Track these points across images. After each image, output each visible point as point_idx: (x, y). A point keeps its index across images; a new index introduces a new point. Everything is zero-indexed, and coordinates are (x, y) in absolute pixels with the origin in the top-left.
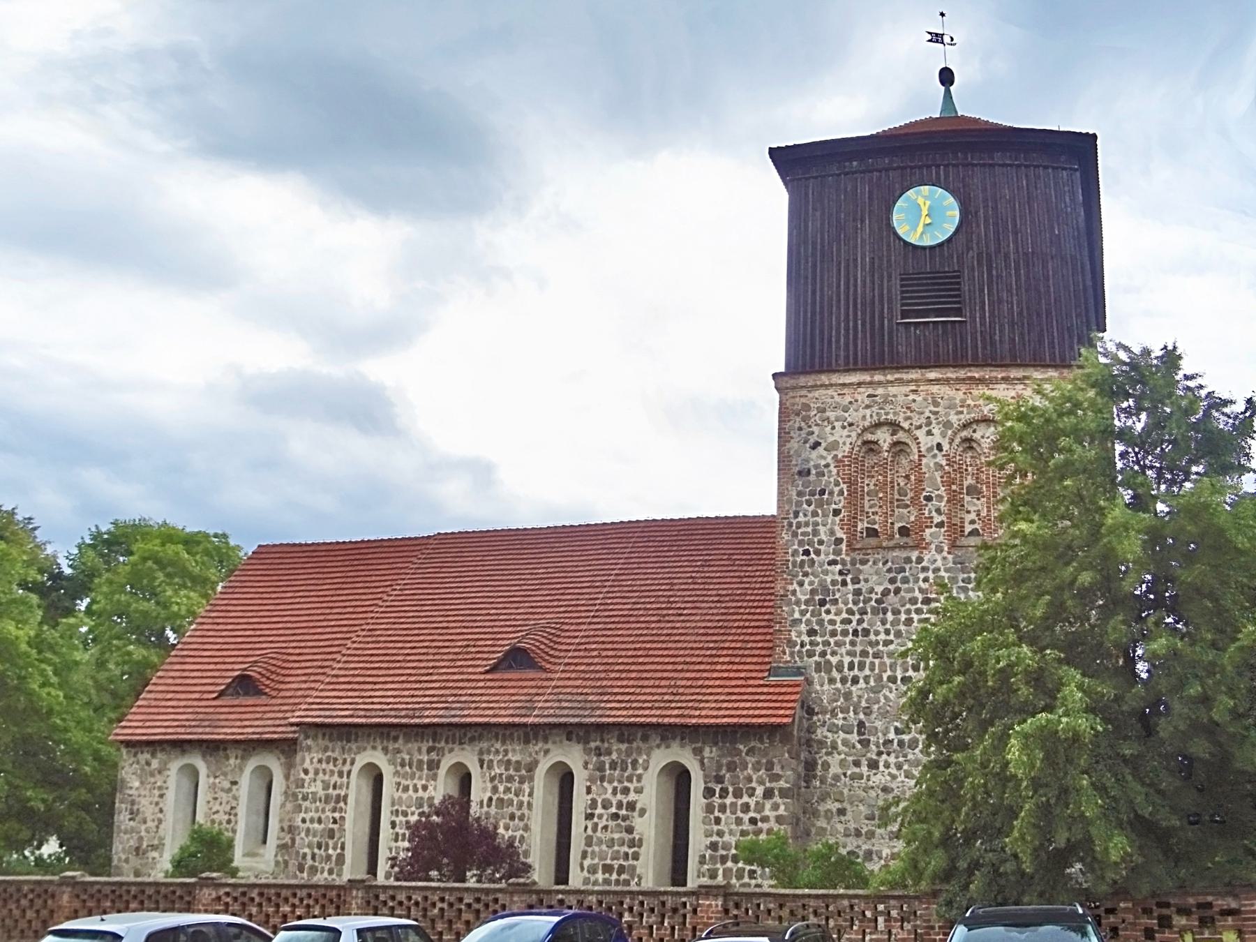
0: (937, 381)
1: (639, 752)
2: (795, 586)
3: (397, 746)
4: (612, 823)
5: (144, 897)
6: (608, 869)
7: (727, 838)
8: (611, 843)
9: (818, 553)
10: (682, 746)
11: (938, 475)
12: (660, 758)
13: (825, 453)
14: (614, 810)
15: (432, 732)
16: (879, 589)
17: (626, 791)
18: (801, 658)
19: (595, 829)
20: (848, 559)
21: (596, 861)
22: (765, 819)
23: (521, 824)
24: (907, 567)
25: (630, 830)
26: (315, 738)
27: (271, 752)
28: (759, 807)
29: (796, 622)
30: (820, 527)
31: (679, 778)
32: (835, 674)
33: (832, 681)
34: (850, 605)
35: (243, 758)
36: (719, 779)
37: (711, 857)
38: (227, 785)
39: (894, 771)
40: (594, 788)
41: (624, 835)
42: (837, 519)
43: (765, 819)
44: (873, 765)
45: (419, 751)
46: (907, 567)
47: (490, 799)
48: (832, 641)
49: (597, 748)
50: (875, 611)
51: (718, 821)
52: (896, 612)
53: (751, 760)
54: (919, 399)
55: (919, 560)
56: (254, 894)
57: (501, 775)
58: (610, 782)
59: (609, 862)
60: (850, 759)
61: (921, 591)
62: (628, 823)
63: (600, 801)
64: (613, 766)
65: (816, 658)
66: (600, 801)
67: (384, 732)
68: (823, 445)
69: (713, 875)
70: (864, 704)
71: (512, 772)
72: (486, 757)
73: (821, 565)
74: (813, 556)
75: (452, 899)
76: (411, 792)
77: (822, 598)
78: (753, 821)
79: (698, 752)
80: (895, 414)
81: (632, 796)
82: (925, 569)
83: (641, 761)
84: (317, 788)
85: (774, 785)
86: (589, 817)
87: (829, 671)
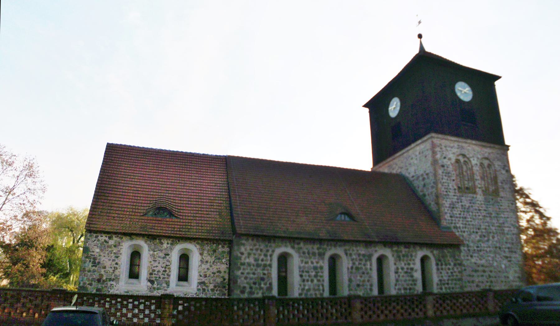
0: (475, 144)
1: (412, 251)
6: (405, 289)
8: (405, 281)
12: (420, 253)
15: (368, 243)
16: (467, 205)
19: (399, 276)
22: (455, 272)
25: (412, 276)
26: (247, 240)
27: (191, 243)
28: (453, 269)
31: (424, 260)
36: (440, 260)
38: (162, 255)
41: (410, 278)
44: (472, 256)
47: (352, 268)
50: (468, 212)
51: (441, 273)
52: (472, 213)
58: (403, 261)
64: (404, 256)
71: (361, 257)
77: (453, 207)
79: (432, 252)
81: (412, 266)
84: (251, 260)
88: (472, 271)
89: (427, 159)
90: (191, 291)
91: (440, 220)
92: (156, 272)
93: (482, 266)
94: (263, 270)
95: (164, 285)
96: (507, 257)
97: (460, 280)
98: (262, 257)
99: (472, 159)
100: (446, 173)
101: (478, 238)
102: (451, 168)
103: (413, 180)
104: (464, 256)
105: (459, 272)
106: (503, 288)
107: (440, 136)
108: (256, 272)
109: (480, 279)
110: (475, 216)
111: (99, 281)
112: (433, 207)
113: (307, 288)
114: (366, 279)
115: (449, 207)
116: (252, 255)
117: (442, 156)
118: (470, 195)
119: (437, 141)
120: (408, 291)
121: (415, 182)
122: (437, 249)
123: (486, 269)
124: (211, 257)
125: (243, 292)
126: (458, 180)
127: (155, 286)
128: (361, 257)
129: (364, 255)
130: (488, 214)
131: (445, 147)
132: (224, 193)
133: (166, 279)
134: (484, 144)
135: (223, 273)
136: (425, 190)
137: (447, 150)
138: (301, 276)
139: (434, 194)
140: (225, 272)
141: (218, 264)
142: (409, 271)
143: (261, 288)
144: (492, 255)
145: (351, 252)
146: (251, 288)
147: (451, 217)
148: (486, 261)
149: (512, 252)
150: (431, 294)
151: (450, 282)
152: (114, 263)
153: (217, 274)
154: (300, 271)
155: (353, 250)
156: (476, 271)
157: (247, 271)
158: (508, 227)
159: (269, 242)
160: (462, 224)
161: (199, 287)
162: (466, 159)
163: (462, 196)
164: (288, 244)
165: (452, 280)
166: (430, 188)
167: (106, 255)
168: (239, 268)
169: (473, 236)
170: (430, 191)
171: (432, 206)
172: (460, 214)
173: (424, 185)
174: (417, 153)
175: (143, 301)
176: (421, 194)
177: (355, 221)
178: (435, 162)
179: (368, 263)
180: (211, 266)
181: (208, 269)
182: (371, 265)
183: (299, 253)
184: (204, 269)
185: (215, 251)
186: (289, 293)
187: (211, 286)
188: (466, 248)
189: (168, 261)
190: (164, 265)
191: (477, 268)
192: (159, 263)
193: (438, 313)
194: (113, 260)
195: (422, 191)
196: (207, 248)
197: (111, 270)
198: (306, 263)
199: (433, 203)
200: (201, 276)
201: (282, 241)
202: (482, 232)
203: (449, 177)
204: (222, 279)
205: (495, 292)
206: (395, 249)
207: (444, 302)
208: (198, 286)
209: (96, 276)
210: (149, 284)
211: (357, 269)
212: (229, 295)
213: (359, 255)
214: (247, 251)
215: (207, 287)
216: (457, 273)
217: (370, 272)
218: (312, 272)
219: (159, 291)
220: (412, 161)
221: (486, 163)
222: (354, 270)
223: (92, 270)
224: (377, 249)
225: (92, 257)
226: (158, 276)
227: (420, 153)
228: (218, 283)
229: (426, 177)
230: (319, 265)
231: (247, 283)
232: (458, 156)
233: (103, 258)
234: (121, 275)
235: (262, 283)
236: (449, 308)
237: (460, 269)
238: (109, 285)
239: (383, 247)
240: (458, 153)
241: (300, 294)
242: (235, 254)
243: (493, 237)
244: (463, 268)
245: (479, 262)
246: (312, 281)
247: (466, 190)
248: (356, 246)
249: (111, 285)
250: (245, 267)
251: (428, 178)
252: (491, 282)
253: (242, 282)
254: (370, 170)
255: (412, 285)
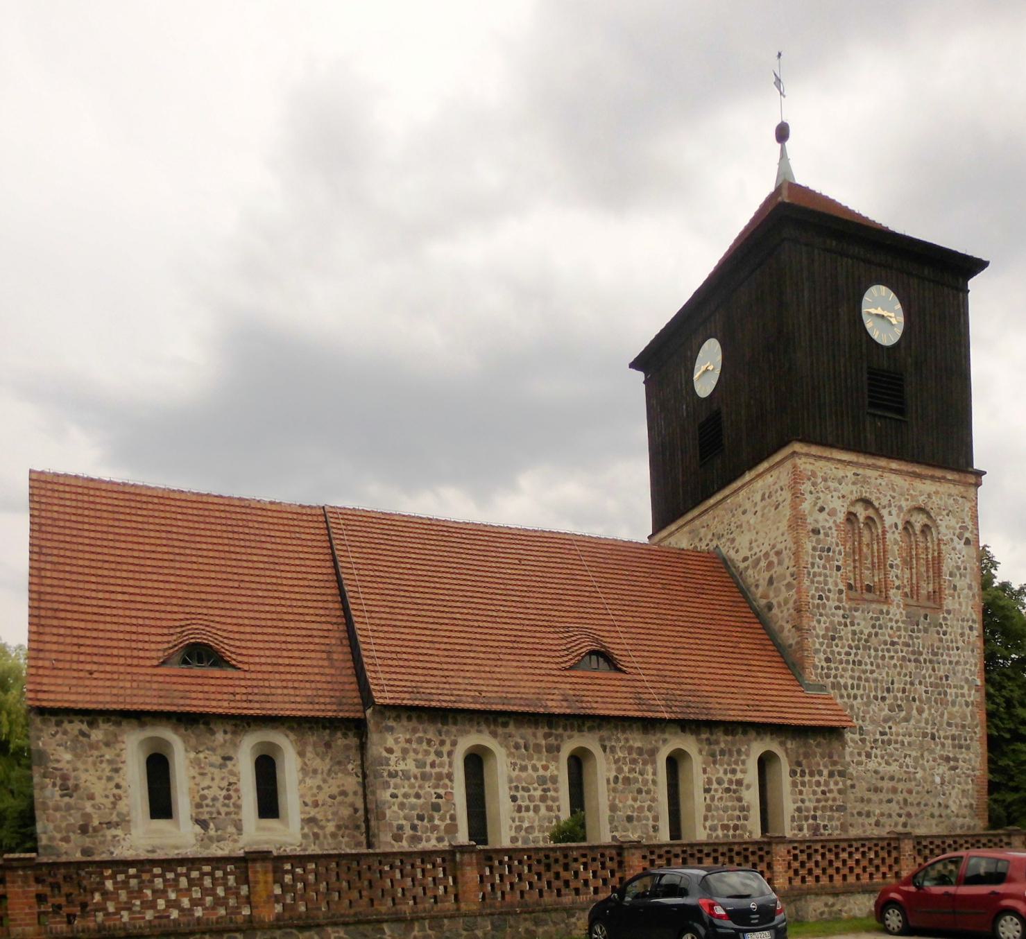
2: (815, 623)
3: (507, 730)
4: (725, 795)
5: (718, 854)
6: (725, 827)
7: (807, 804)
8: (725, 809)
9: (828, 599)
10: (772, 739)
11: (896, 548)
12: (758, 747)
13: (828, 517)
14: (726, 785)
15: (649, 725)
16: (866, 632)
17: (734, 772)
18: (822, 678)
19: (712, 799)
20: (847, 606)
21: (716, 822)
22: (831, 791)
23: (649, 797)
24: (881, 617)
25: (740, 799)
27: (277, 728)
28: (827, 783)
29: (817, 651)
30: (828, 579)
31: (765, 762)
32: (843, 691)
33: (842, 697)
34: (850, 642)
35: (234, 733)
36: (799, 764)
37: (799, 817)
38: (216, 759)
39: (879, 760)
40: (708, 769)
41: (737, 804)
42: (839, 573)
43: (831, 791)
44: (868, 756)
45: (538, 736)
46: (881, 617)
47: (616, 778)
48: (840, 667)
49: (708, 739)
50: (865, 648)
51: (801, 793)
52: (876, 650)
53: (818, 750)
54: (884, 483)
55: (888, 613)
56: (818, 846)
57: (624, 758)
58: (721, 765)
59: (726, 822)
60: (856, 751)
61: (890, 636)
62: (737, 794)
63: (714, 779)
64: (722, 753)
65: (832, 679)
66: (714, 779)
67: (687, 725)
68: (827, 510)
69: (801, 829)
70: (861, 714)
71: (634, 756)
72: (607, 743)
73: (831, 609)
74: (825, 600)
75: (973, 841)
76: (530, 771)
78: (824, 793)
79: (782, 744)
80: (870, 493)
81: (739, 776)
82: (891, 620)
83: (743, 750)
84: (410, 765)
85: (834, 768)
86: (707, 791)
87: (840, 689)
88: (869, 790)
89: (799, 508)
90: (289, 840)
91: (803, 668)
92: (209, 801)
93: (892, 778)
94: (437, 786)
95: (231, 829)
96: (948, 759)
97: (841, 808)
98: (432, 757)
99: (884, 512)
100: (822, 550)
101: (886, 712)
102: (833, 539)
103: (747, 568)
104: (851, 754)
105: (840, 792)
106: (935, 831)
107: (815, 450)
108: (422, 792)
109: (885, 808)
110: (883, 657)
111: (84, 829)
112: (789, 636)
113: (526, 825)
114: (646, 805)
115: (824, 637)
116: (412, 754)
117: (815, 504)
118: (874, 606)
119: (804, 465)
120: (731, 832)
121: (750, 572)
122: (794, 738)
123: (900, 786)
124: (323, 759)
125: (398, 838)
126: (850, 568)
127: (212, 832)
128: (634, 756)
129: (640, 751)
130: (913, 653)
131: (825, 480)
132: (331, 605)
133: (233, 816)
134: (918, 469)
135: (351, 794)
136: (772, 594)
137: (828, 488)
138: (514, 799)
139: (791, 604)
140: (355, 793)
141: (340, 775)
142: (734, 787)
143: (435, 828)
144: (914, 754)
145: (613, 744)
146: (414, 827)
147: (828, 660)
148: (901, 767)
149: (961, 747)
150: (782, 840)
151: (819, 813)
152: (112, 785)
153: (339, 799)
154: (510, 788)
155: (618, 740)
156: (877, 790)
157: (403, 790)
158: (955, 687)
159: (445, 723)
160: (852, 678)
161: (306, 830)
162: (871, 512)
163: (856, 610)
164: (483, 727)
165: (824, 808)
166: (783, 589)
167: (90, 767)
168: (386, 785)
169: (874, 707)
170: (784, 594)
171: (786, 633)
172: (848, 654)
173: (771, 581)
174: (758, 497)
175: (184, 870)
176: (763, 602)
177: (620, 670)
178: (797, 521)
179: (649, 768)
180: (325, 781)
181: (319, 788)
182: (654, 774)
183: (507, 747)
184: (311, 788)
185: (328, 745)
186: (490, 839)
187: (331, 827)
188: (857, 737)
189: (232, 773)
190: (224, 784)
191: (880, 784)
192: (213, 779)
193: (797, 882)
194: (109, 779)
195: (765, 596)
196: (312, 738)
197: (108, 802)
198: (524, 768)
199: (788, 627)
200: (306, 804)
201: (471, 720)
202: (896, 698)
203: (828, 559)
204: (350, 810)
205: (918, 840)
206: (704, 736)
207: (809, 857)
208: (302, 828)
209: (75, 819)
210: (198, 829)
211: (627, 781)
212: (370, 845)
213: (630, 749)
214: (395, 746)
215: (322, 828)
216: (836, 794)
217: (652, 787)
218: (535, 789)
219: (221, 844)
220: (744, 518)
221: (919, 520)
222: (620, 786)
223: (62, 804)
224: (666, 736)
225: (58, 773)
226: (213, 810)
227: (763, 499)
228: (343, 818)
229: (775, 559)
230: (548, 774)
231: (405, 818)
232: (853, 503)
233: (83, 776)
234: (133, 814)
235: (436, 815)
236: (818, 872)
237: (841, 786)
238: (109, 838)
239: (679, 731)
240: (854, 497)
241: (514, 840)
242: (375, 752)
243: (920, 711)
244: (849, 782)
245: (883, 769)
246: (536, 809)
247: (868, 592)
248: (624, 731)
249: (114, 837)
250: (398, 780)
251: (780, 563)
252: (909, 815)
253: (394, 815)
254: (646, 541)
255: (739, 818)
